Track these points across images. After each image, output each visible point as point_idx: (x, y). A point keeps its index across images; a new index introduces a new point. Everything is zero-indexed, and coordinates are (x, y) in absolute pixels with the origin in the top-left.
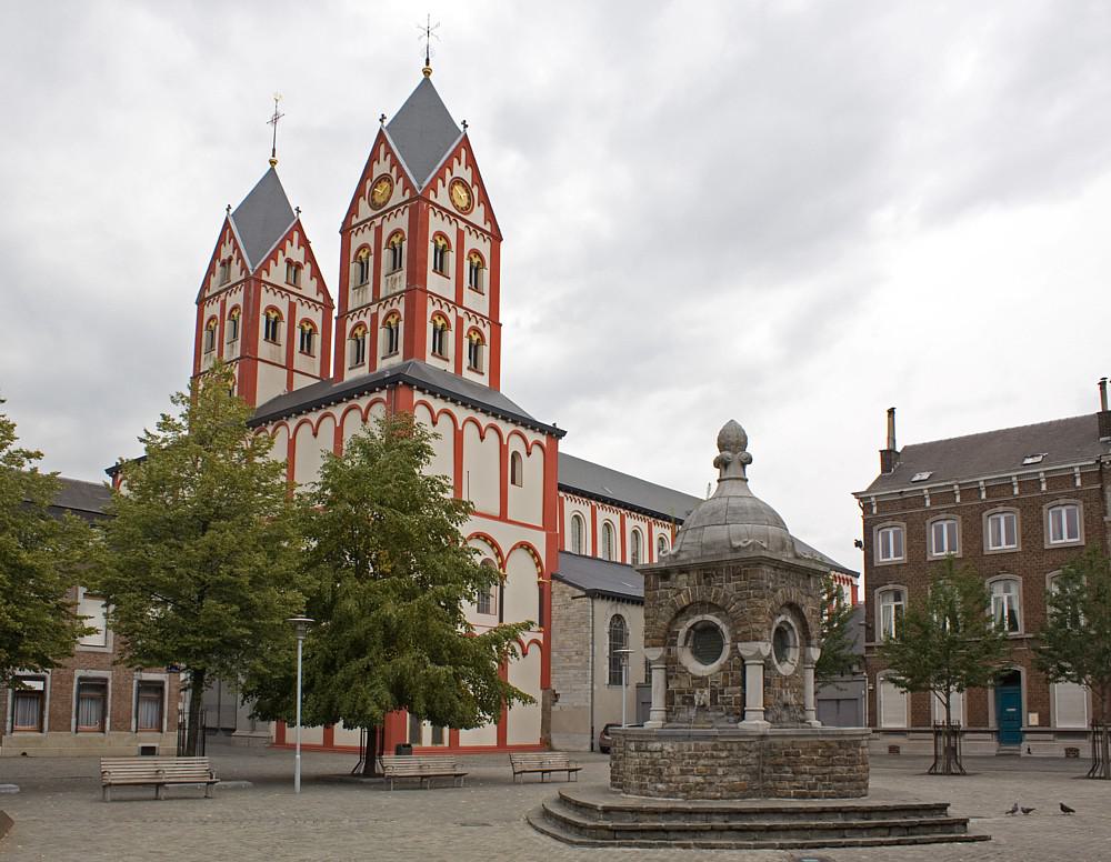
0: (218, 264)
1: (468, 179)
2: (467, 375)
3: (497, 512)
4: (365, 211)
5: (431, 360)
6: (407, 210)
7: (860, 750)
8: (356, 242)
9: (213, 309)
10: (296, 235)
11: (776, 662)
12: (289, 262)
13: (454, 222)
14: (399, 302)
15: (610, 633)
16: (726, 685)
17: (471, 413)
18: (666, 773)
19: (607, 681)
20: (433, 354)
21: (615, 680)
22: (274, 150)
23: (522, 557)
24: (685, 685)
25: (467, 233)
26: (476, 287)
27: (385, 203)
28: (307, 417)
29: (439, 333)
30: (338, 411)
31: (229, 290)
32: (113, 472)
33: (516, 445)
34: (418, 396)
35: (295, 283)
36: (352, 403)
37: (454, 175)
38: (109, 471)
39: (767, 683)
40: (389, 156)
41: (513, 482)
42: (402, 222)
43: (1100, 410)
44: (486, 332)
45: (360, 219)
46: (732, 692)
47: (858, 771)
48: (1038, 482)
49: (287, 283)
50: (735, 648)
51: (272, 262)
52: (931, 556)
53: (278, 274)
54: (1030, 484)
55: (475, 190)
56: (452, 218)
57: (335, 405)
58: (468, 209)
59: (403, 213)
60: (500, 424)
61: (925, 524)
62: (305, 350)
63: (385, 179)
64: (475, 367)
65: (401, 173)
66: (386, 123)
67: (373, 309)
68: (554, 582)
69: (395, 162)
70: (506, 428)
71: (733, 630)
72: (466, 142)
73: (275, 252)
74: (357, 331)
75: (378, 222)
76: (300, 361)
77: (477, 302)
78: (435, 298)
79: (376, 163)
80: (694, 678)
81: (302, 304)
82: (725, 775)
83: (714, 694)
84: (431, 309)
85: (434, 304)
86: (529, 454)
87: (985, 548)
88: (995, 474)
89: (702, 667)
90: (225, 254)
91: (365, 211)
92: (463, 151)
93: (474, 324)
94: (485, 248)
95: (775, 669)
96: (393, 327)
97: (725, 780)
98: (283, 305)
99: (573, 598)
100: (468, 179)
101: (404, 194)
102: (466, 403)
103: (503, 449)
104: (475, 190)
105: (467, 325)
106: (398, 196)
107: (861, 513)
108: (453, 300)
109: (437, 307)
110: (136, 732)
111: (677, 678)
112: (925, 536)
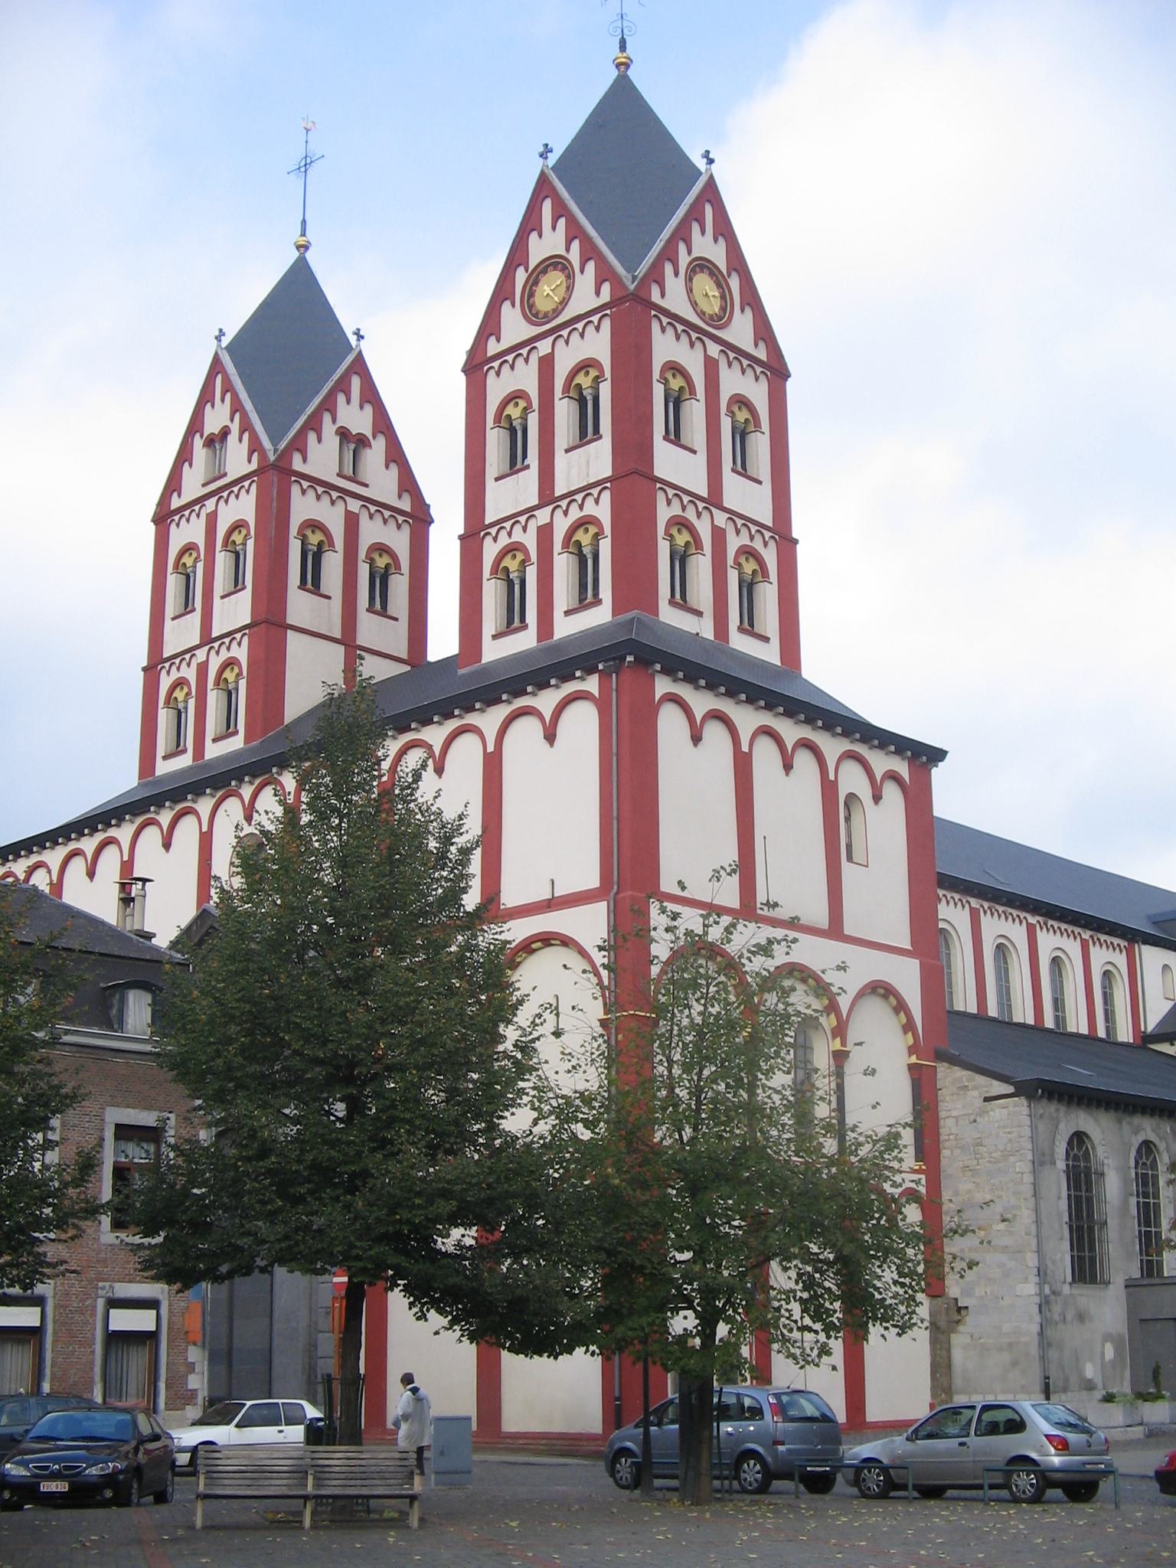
0: (198, 442)
2: (740, 642)
4: (514, 327)
8: (497, 389)
9: (188, 532)
10: (356, 382)
12: (344, 434)
13: (698, 345)
15: (1067, 1172)
17: (766, 719)
19: (1069, 1279)
20: (672, 602)
21: (1082, 1270)
22: (304, 222)
26: (742, 469)
27: (557, 312)
30: (489, 720)
31: (223, 491)
33: (852, 780)
34: (663, 686)
37: (695, 254)
40: (562, 222)
41: (850, 859)
42: (597, 344)
44: (770, 556)
45: (505, 344)
51: (312, 437)
55: (734, 283)
56: (694, 335)
57: (482, 710)
58: (722, 319)
59: (248, 491)
60: (823, 740)
63: (555, 266)
64: (749, 627)
66: (553, 159)
67: (201, 655)
68: (942, 1068)
70: (832, 747)
72: (711, 192)
74: (581, 536)
75: (544, 347)
76: (370, 630)
78: (671, 492)
79: (534, 236)
81: (371, 516)
84: (664, 513)
86: (877, 798)
91: (514, 327)
92: (709, 210)
94: (758, 393)
96: (587, 550)
98: (333, 518)
99: (987, 1099)
101: (598, 293)
103: (829, 788)
104: (734, 283)
105: (734, 543)
106: (586, 295)
108: (705, 494)
109: (676, 510)
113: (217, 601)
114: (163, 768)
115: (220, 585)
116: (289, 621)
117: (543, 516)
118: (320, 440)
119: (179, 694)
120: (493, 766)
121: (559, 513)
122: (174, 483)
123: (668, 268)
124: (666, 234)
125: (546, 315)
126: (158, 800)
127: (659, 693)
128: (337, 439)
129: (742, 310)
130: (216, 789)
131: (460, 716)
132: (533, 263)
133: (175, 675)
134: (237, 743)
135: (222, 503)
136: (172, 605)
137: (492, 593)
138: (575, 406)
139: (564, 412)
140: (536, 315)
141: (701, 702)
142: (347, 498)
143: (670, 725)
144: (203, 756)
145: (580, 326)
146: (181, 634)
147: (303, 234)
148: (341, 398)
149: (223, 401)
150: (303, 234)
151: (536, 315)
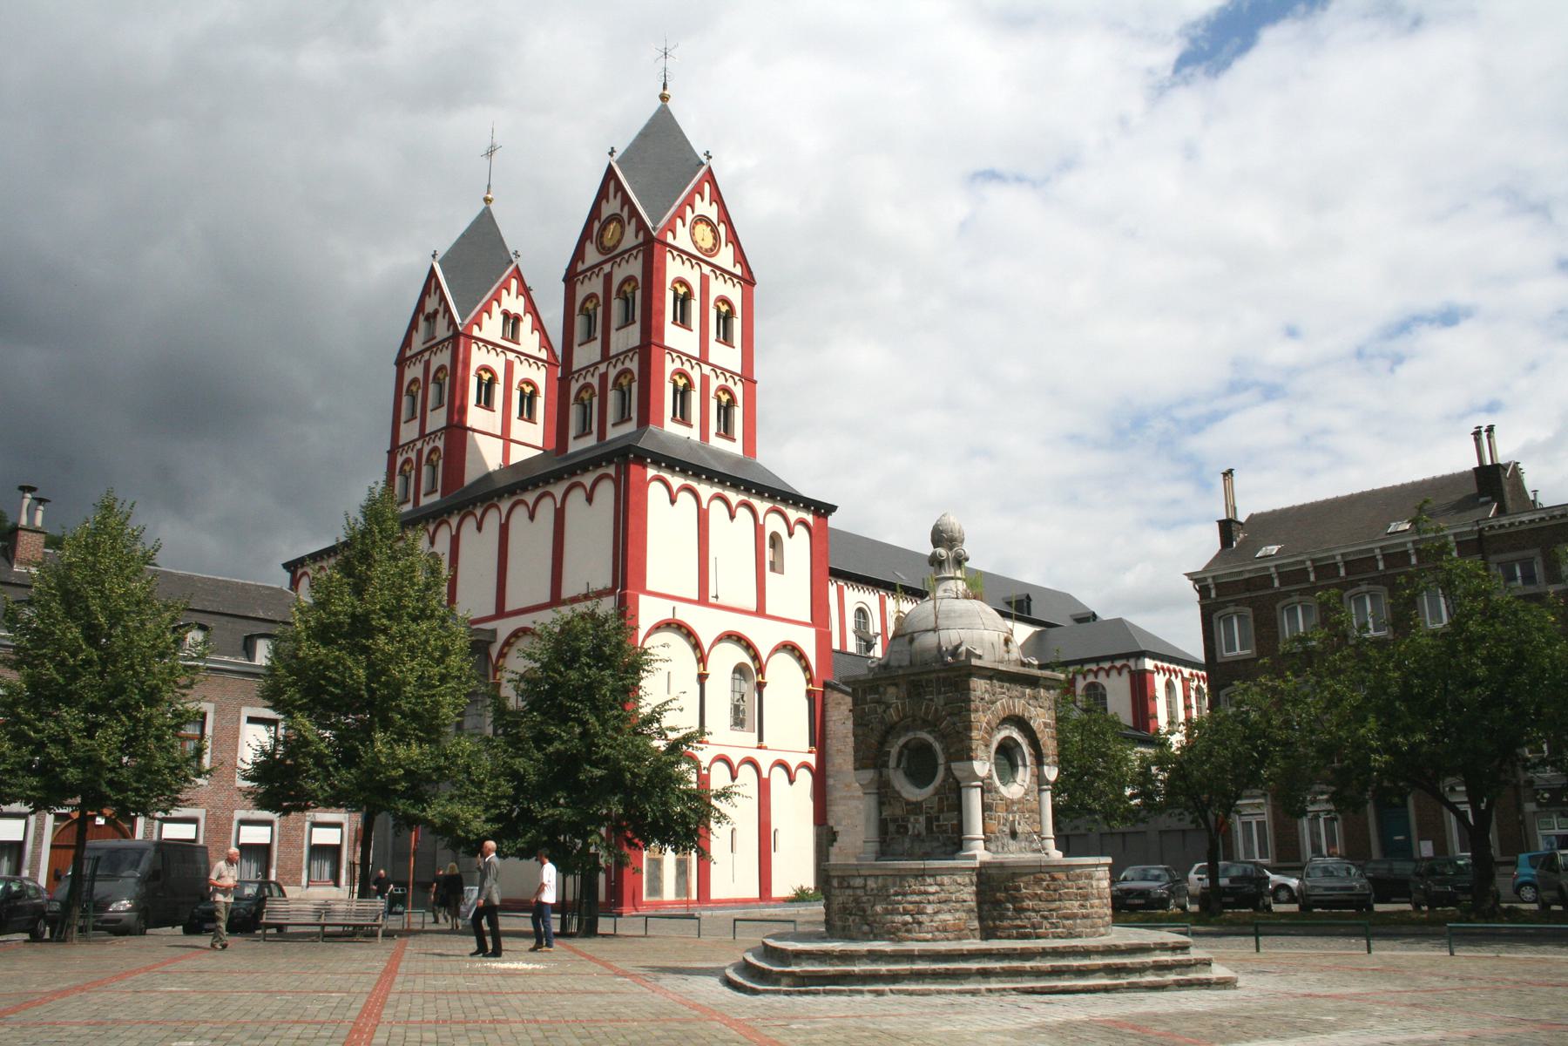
0: (421, 318)
1: (714, 217)
2: (717, 443)
3: (753, 607)
4: (592, 256)
5: (671, 428)
6: (443, 437)
7: (1094, 883)
8: (581, 292)
9: (414, 371)
10: (514, 283)
11: (998, 783)
12: (506, 314)
13: (696, 267)
14: (631, 360)
16: (941, 811)
18: (869, 912)
20: (674, 418)
22: (489, 186)
23: (786, 661)
24: (898, 812)
25: (712, 276)
26: (726, 339)
27: (615, 247)
28: (521, 498)
29: (682, 395)
30: (558, 490)
32: (293, 567)
35: (515, 338)
36: (575, 479)
37: (697, 213)
38: (287, 566)
39: (986, 808)
42: (634, 268)
43: (1477, 465)
44: (738, 390)
46: (948, 820)
47: (1092, 907)
48: (1270, 578)
49: (503, 338)
50: (948, 770)
51: (485, 315)
52: (1222, 657)
53: (492, 328)
54: (1396, 558)
55: (722, 229)
58: (713, 251)
59: (636, 258)
60: (755, 502)
61: (1274, 609)
62: (525, 416)
65: (634, 212)
66: (617, 156)
67: (602, 368)
69: (626, 200)
70: (762, 506)
71: (946, 750)
72: (710, 177)
73: (479, 315)
75: (607, 268)
76: (519, 429)
77: (727, 357)
78: (674, 355)
79: (604, 201)
80: (908, 803)
81: (521, 362)
82: (936, 913)
83: (929, 821)
84: (670, 366)
85: (673, 361)
86: (791, 534)
87: (1218, 655)
88: (1353, 546)
89: (917, 791)
90: (429, 308)
91: (592, 256)
92: (707, 186)
93: (723, 382)
94: (735, 294)
95: (997, 791)
97: (936, 918)
98: (497, 363)
100: (714, 217)
101: (637, 237)
102: (711, 476)
103: (759, 529)
104: (722, 229)
105: (714, 384)
107: (1197, 596)
108: (697, 355)
109: (677, 365)
110: (308, 886)
111: (890, 804)
112: (1276, 623)
113: (429, 413)
114: (574, 446)
115: (430, 404)
116: (468, 425)
117: (602, 368)
118: (490, 318)
119: (407, 468)
120: (455, 542)
121: (611, 366)
122: (407, 342)
123: (679, 221)
124: (678, 202)
125: (609, 248)
126: (557, 476)
127: (649, 477)
128: (502, 317)
129: (726, 245)
130: (459, 510)
131: (543, 486)
132: (604, 217)
133: (405, 456)
134: (436, 497)
135: (616, 266)
136: (404, 415)
137: (574, 412)
138: (623, 302)
139: (616, 306)
140: (604, 248)
141: (676, 481)
142: (701, 264)
143: (656, 493)
144: (566, 449)
145: (626, 256)
146: (409, 432)
147: (488, 192)
148: (504, 292)
149: (615, 197)
150: (488, 192)
151: (604, 248)
